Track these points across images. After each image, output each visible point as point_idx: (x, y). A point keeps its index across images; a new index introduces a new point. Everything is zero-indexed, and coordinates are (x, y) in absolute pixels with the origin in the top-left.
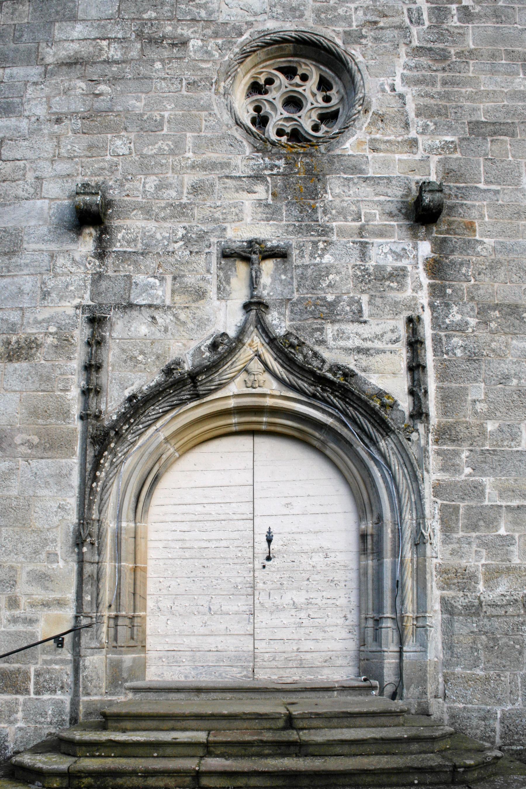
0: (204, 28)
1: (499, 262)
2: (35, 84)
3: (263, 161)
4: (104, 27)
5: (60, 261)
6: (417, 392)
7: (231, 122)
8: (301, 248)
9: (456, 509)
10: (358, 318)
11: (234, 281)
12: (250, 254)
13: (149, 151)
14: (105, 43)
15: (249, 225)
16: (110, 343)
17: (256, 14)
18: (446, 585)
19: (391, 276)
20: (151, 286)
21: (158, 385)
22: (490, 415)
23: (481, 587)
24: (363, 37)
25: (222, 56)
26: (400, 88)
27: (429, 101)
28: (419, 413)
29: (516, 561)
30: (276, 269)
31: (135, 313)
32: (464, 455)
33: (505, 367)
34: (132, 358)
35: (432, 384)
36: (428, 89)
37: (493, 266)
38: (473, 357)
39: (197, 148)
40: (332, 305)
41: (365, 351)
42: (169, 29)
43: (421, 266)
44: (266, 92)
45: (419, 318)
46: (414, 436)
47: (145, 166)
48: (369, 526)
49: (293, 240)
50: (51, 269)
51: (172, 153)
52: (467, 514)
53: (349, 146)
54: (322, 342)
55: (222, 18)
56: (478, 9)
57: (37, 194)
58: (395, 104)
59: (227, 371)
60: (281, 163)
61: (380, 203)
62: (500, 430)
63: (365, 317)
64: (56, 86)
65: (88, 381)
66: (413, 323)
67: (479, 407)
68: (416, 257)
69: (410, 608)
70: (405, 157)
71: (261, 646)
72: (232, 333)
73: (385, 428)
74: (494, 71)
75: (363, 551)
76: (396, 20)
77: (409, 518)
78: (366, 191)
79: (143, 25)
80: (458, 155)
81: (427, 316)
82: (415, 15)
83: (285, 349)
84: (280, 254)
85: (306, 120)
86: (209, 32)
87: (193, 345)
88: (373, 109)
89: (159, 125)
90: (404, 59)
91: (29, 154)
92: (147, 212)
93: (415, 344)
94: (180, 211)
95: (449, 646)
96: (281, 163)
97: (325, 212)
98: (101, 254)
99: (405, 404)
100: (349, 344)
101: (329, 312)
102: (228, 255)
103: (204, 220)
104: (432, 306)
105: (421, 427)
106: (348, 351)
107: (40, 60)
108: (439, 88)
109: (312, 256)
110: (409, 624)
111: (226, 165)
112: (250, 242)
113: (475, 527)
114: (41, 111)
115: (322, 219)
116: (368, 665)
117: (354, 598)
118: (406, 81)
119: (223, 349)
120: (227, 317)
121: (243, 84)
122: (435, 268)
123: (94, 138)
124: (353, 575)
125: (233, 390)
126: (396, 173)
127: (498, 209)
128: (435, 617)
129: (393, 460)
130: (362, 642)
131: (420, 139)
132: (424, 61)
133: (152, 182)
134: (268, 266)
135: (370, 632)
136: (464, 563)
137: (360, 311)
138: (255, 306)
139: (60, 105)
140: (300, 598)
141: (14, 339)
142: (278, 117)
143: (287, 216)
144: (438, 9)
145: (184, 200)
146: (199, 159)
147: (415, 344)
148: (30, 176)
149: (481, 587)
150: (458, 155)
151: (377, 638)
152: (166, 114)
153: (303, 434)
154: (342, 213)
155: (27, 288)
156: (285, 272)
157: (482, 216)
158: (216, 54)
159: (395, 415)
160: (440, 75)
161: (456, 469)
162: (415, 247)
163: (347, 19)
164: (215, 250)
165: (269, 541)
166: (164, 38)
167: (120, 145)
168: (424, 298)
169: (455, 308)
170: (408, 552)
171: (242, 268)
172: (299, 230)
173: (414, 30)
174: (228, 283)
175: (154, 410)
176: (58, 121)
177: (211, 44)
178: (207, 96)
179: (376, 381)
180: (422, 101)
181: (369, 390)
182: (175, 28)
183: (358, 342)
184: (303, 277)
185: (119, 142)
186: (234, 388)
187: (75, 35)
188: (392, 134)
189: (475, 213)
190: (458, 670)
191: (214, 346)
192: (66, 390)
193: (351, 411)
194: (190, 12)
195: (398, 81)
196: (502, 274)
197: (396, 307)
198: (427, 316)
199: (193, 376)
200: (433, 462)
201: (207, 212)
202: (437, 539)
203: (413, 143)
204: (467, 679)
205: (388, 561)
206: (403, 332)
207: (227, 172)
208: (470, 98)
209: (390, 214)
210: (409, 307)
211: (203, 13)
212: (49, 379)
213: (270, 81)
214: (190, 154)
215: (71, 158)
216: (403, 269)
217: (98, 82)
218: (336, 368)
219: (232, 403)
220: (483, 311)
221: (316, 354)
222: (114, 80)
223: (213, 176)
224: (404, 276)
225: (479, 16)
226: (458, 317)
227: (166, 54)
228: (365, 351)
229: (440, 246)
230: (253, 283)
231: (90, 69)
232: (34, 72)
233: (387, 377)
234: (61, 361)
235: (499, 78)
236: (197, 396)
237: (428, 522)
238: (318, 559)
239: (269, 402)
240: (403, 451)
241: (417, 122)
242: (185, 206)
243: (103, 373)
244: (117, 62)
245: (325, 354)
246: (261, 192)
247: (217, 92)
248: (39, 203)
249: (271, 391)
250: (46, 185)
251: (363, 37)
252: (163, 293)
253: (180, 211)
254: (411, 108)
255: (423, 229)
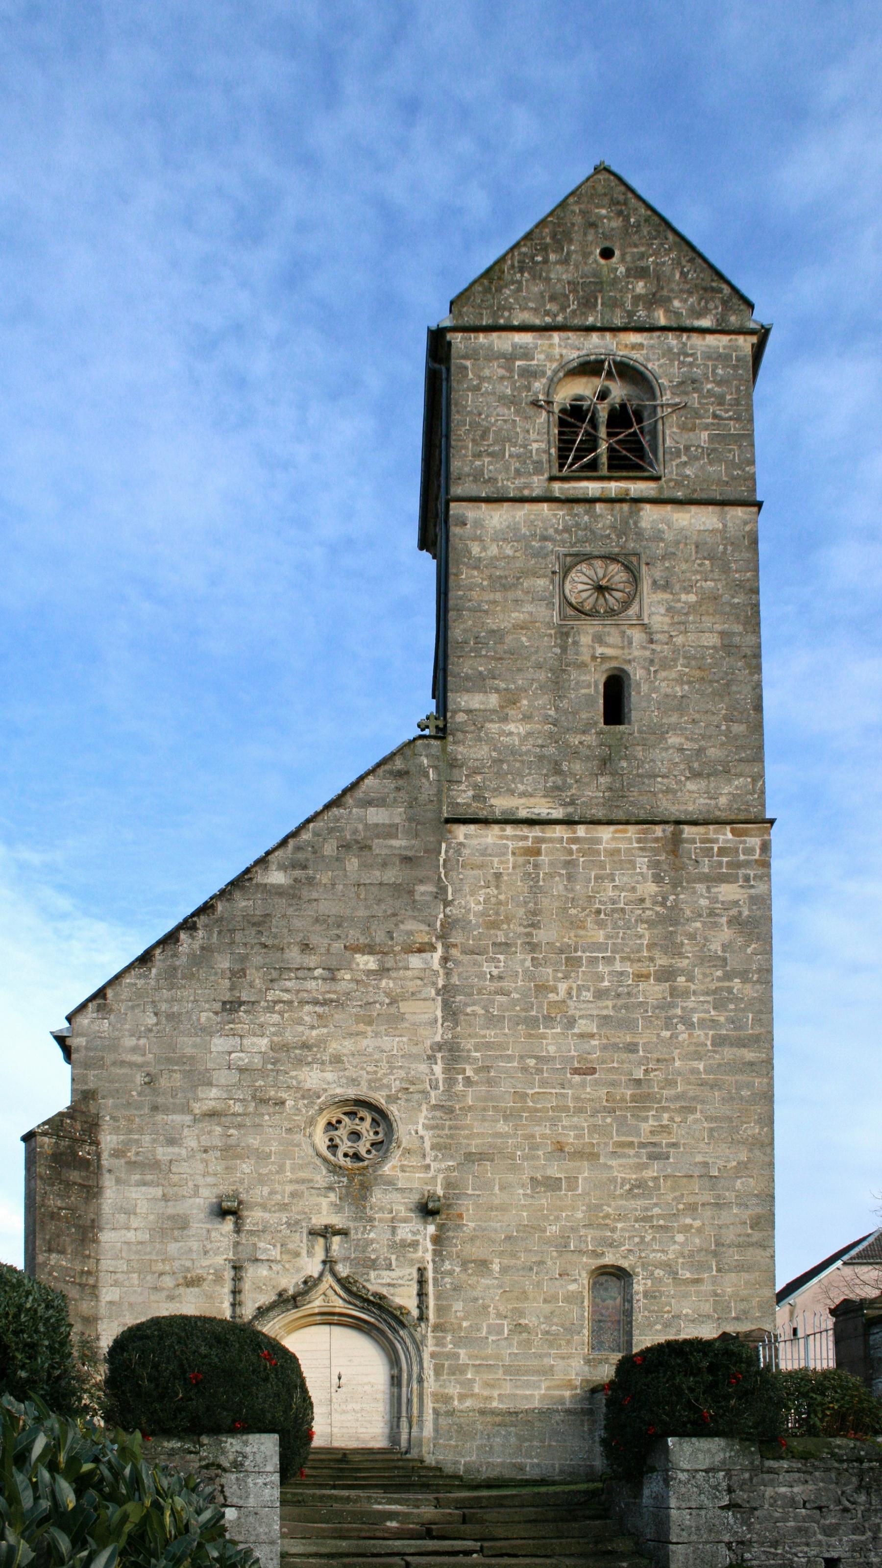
0: (295, 1092)
1: (477, 1237)
2: (189, 1126)
3: (333, 1178)
4: (230, 1091)
5: (213, 1234)
6: (422, 1306)
7: (314, 1154)
8: (356, 1229)
9: (443, 1365)
10: (389, 1267)
11: (316, 1247)
12: (326, 1232)
13: (264, 1171)
14: (232, 1102)
15: (326, 1214)
16: (246, 1279)
17: (329, 1083)
18: (436, 1401)
19: (409, 1245)
20: (267, 1248)
21: (274, 1302)
22: (465, 1318)
23: (456, 1403)
24: (399, 1099)
25: (307, 1112)
26: (421, 1132)
27: (439, 1140)
28: (422, 1318)
29: (476, 1390)
30: (342, 1241)
31: (259, 1264)
32: (449, 1338)
33: (475, 1294)
34: (259, 1287)
35: (431, 1302)
36: (440, 1132)
37: (472, 1239)
38: (457, 1288)
39: (293, 1170)
40: (374, 1261)
41: (393, 1285)
42: (272, 1093)
43: (428, 1239)
44: (336, 1129)
45: (425, 1269)
46: (419, 1329)
47: (262, 1180)
48: (395, 1372)
49: (351, 1225)
50: (208, 1238)
51: (278, 1172)
52: (447, 1367)
53: (387, 1169)
54: (368, 1280)
55: (307, 1086)
56: (476, 1078)
57: (196, 1194)
58: (417, 1143)
59: (313, 1294)
60: (345, 1179)
61: (405, 1203)
62: (471, 1326)
63: (394, 1267)
64: (202, 1129)
65: (234, 1299)
66: (421, 1271)
67: (458, 1314)
68: (425, 1234)
69: (415, 1411)
70: (422, 1175)
71: (335, 1430)
72: (316, 1275)
73: (403, 1325)
74: (484, 1119)
75: (392, 1384)
76: (420, 1087)
77: (415, 1369)
78: (396, 1196)
79: (256, 1090)
80: (456, 1174)
81: (430, 1267)
82: (434, 1083)
83: (345, 1284)
84: (343, 1233)
85: (362, 1148)
86: (299, 1095)
87: (294, 1281)
88: (403, 1146)
89: (269, 1155)
90: (425, 1112)
91: (189, 1171)
92: (264, 1207)
93: (422, 1282)
94: (284, 1207)
95: (436, 1430)
96: (345, 1179)
97: (371, 1209)
98: (238, 1230)
99: (415, 1313)
100: (384, 1281)
101: (373, 1264)
102: (313, 1233)
103: (298, 1213)
104: (434, 1261)
105: (423, 1325)
106: (383, 1285)
107: (190, 1111)
108: (447, 1132)
109: (363, 1233)
110: (415, 1420)
111: (311, 1181)
112: (326, 1226)
113: (454, 1374)
114: (193, 1144)
115: (369, 1212)
116: (394, 1437)
117: (388, 1407)
118: (426, 1127)
119: (310, 1284)
120: (313, 1267)
121: (322, 1123)
122: (437, 1240)
123: (231, 1163)
124: (387, 1396)
125: (317, 1303)
126: (416, 1185)
127: (478, 1206)
128: (429, 1416)
129: (408, 1341)
130: (392, 1428)
131: (432, 1164)
132: (438, 1114)
133: (266, 1190)
134: (336, 1239)
135: (395, 1423)
136: (446, 1391)
137: (391, 1264)
138: (328, 1262)
139: (205, 1141)
140: (357, 1407)
141: (189, 1276)
142: (345, 1146)
143: (348, 1211)
144: (450, 1079)
145: (286, 1201)
146: (294, 1177)
147: (422, 1282)
148: (190, 1184)
149: (456, 1403)
150: (456, 1174)
151: (398, 1426)
152: (273, 1149)
153: (358, 1325)
154: (381, 1209)
155: (195, 1248)
156: (347, 1242)
157: (468, 1210)
158: (304, 1111)
159: (409, 1318)
160: (448, 1123)
161: (444, 1345)
162: (425, 1229)
163: (389, 1087)
164: (305, 1231)
165: (340, 1378)
166: (269, 1099)
167: (246, 1167)
168: (429, 1257)
169: (447, 1262)
170: (415, 1386)
171: (321, 1240)
172: (355, 1219)
173: (433, 1093)
174: (313, 1247)
175: (271, 1314)
176: (206, 1151)
177: (301, 1103)
178: (298, 1137)
179: (398, 1301)
180: (435, 1141)
181: (394, 1305)
182: (277, 1092)
183: (388, 1281)
184: (357, 1245)
185: (244, 1166)
186: (317, 1303)
187: (212, 1095)
188: (414, 1161)
189: (464, 1208)
190: (441, 1441)
191: (305, 1282)
192: (222, 1303)
193: (384, 1316)
194: (286, 1082)
195: (420, 1127)
196: (478, 1243)
197: (412, 1262)
198: (430, 1267)
199: (294, 1298)
200: (430, 1341)
201: (300, 1208)
202: (432, 1379)
203: (428, 1167)
204: (445, 1446)
205: (404, 1389)
206: (415, 1275)
207: (311, 1185)
208: (467, 1137)
209: (411, 1210)
210: (420, 1262)
211: (294, 1083)
212: (211, 1297)
213: (339, 1122)
214: (288, 1174)
215: (215, 1175)
216: (418, 1241)
217: (229, 1128)
218: (375, 1294)
219: (317, 1310)
220: (464, 1264)
221: (364, 1287)
222: (240, 1126)
223: (303, 1187)
224: (418, 1245)
225: (477, 1083)
226: (449, 1267)
227: (271, 1110)
228: (393, 1285)
229: (441, 1227)
230: (327, 1250)
231: (223, 1119)
232: (188, 1119)
233: (405, 1298)
234: (218, 1288)
235: (486, 1124)
236: (297, 1307)
237: (426, 1371)
238: (367, 1388)
239: (338, 1310)
240: (412, 1336)
241: (430, 1154)
242: (286, 1205)
243: (242, 1294)
244: (239, 1115)
245: (369, 1286)
246: (333, 1197)
247: (304, 1135)
248: (198, 1200)
249: (338, 1304)
250: (201, 1190)
251: (399, 1099)
252: (275, 1253)
253: (284, 1207)
254: (427, 1145)
255: (431, 1218)
